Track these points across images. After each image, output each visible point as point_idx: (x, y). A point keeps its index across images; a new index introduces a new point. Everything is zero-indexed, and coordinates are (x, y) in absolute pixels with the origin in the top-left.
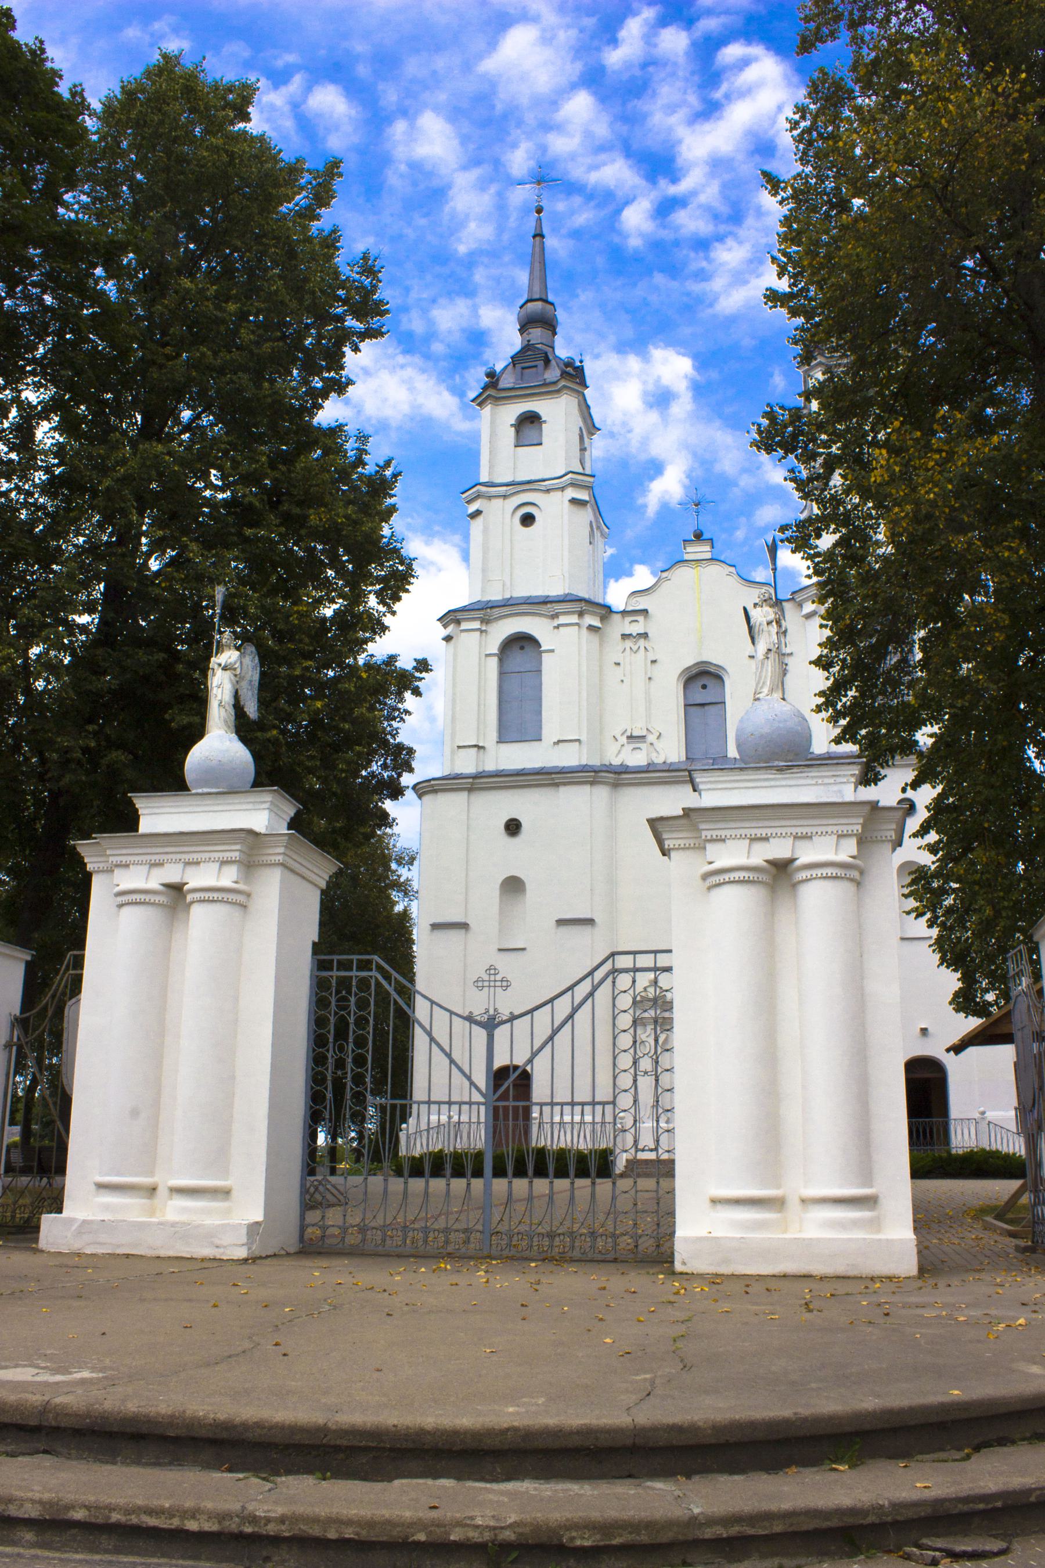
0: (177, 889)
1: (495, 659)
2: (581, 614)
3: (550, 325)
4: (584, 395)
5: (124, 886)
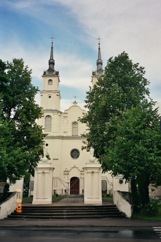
0: (43, 172)
1: (45, 119)
2: (58, 113)
3: (53, 64)
4: (59, 78)
5: (39, 172)
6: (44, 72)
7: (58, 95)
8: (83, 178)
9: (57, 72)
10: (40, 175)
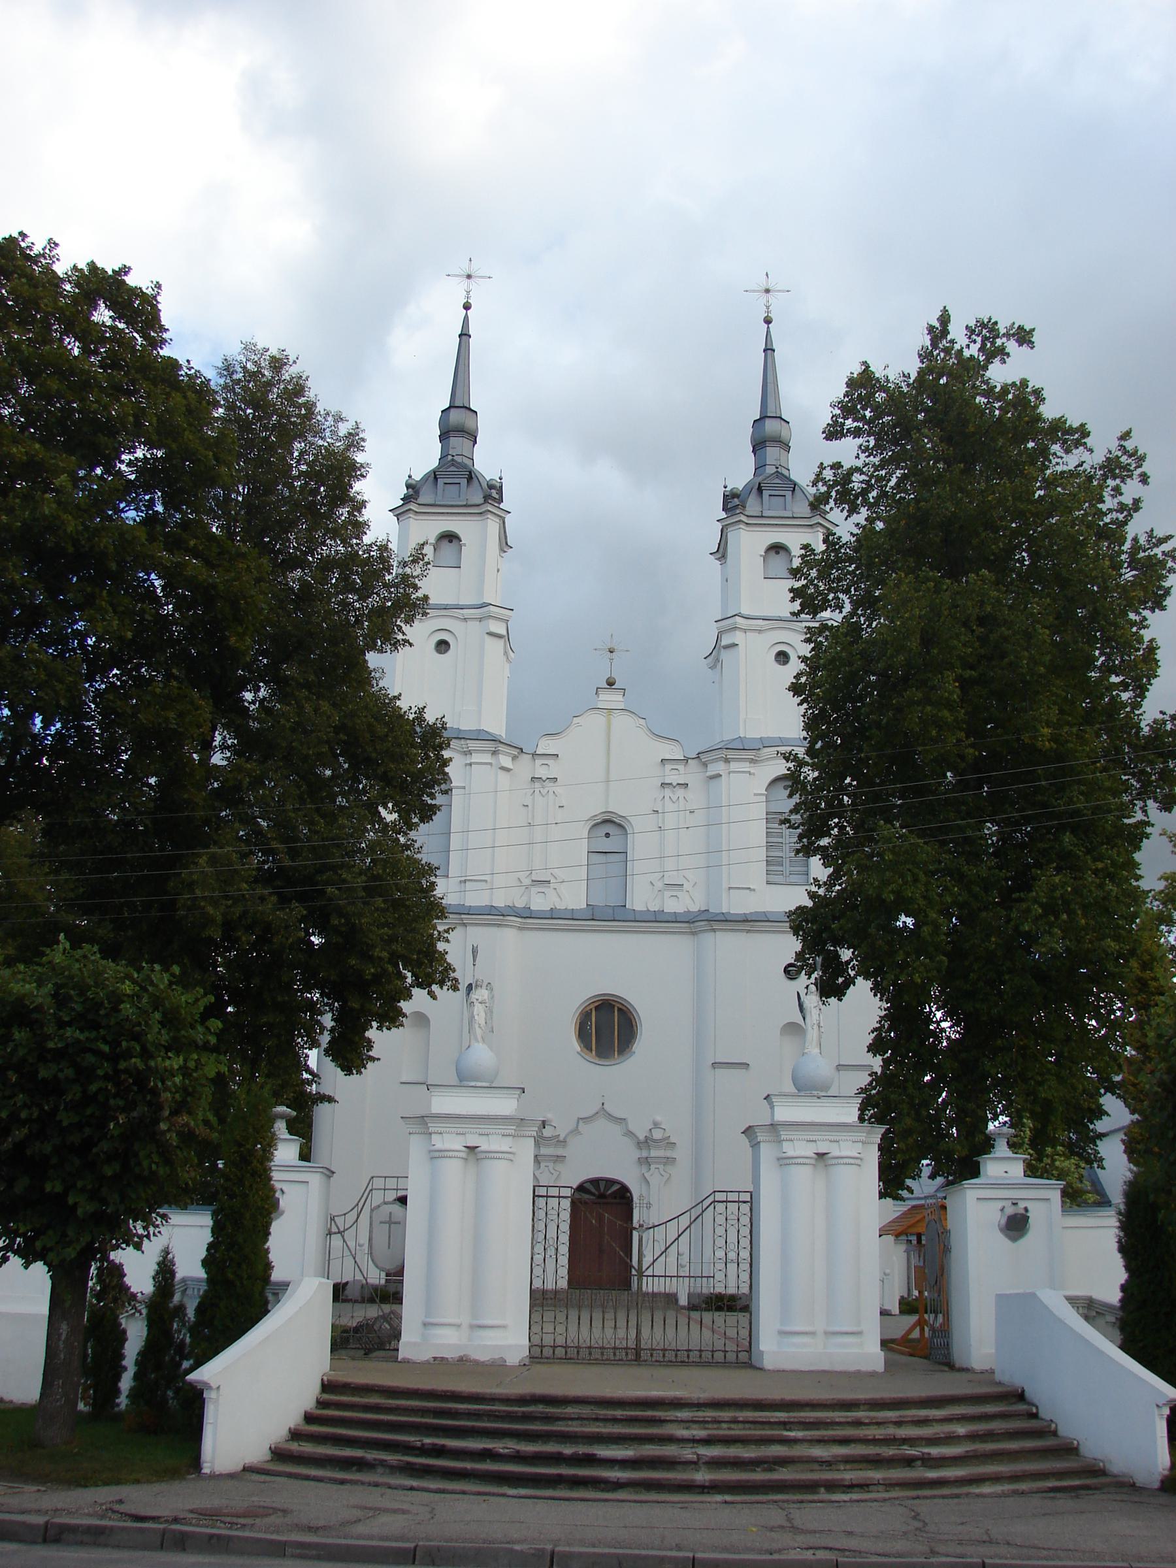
0: (472, 1149)
2: (495, 753)
6: (408, 486)
7: (499, 636)
8: (747, 1197)
9: (491, 487)
10: (802, 1176)
